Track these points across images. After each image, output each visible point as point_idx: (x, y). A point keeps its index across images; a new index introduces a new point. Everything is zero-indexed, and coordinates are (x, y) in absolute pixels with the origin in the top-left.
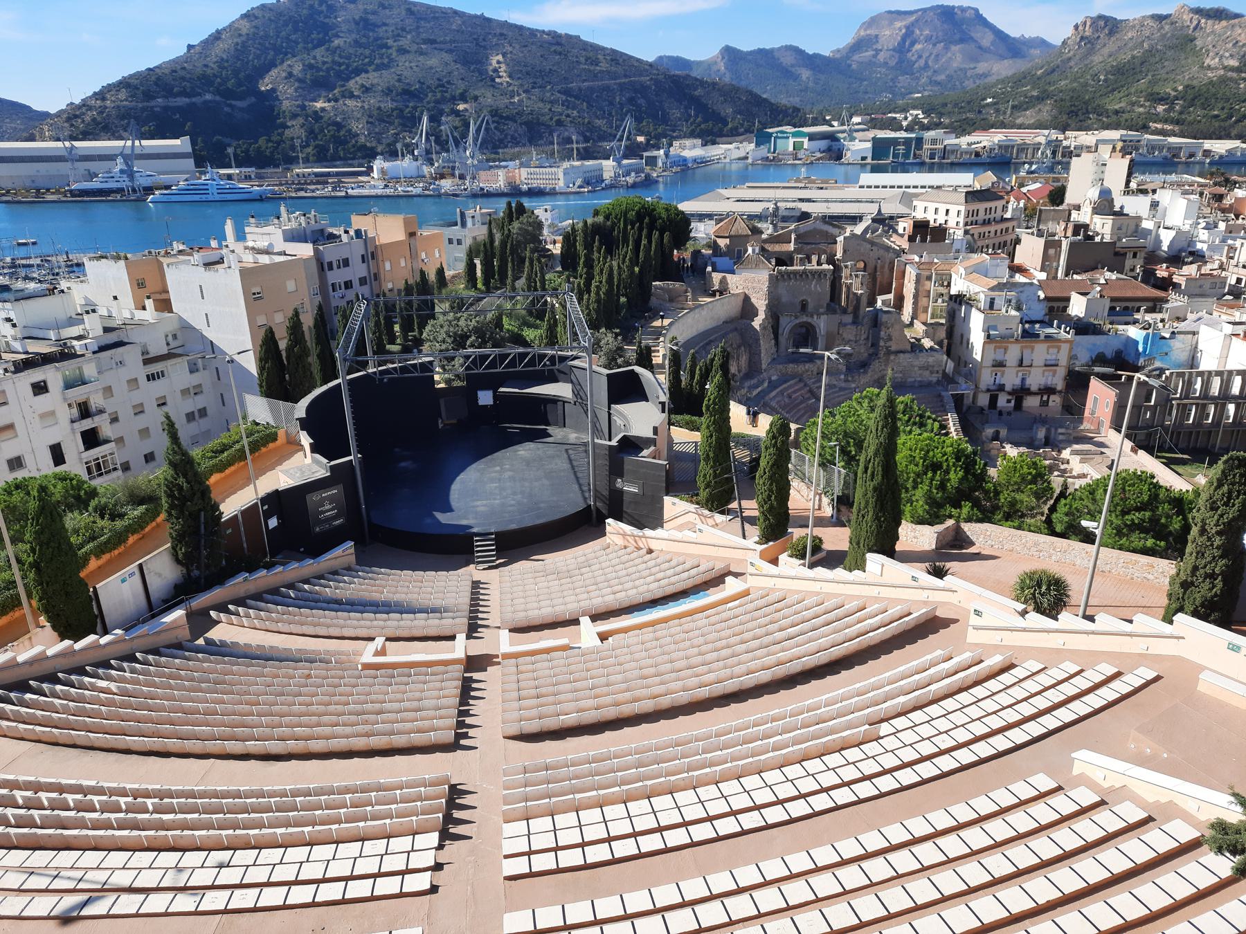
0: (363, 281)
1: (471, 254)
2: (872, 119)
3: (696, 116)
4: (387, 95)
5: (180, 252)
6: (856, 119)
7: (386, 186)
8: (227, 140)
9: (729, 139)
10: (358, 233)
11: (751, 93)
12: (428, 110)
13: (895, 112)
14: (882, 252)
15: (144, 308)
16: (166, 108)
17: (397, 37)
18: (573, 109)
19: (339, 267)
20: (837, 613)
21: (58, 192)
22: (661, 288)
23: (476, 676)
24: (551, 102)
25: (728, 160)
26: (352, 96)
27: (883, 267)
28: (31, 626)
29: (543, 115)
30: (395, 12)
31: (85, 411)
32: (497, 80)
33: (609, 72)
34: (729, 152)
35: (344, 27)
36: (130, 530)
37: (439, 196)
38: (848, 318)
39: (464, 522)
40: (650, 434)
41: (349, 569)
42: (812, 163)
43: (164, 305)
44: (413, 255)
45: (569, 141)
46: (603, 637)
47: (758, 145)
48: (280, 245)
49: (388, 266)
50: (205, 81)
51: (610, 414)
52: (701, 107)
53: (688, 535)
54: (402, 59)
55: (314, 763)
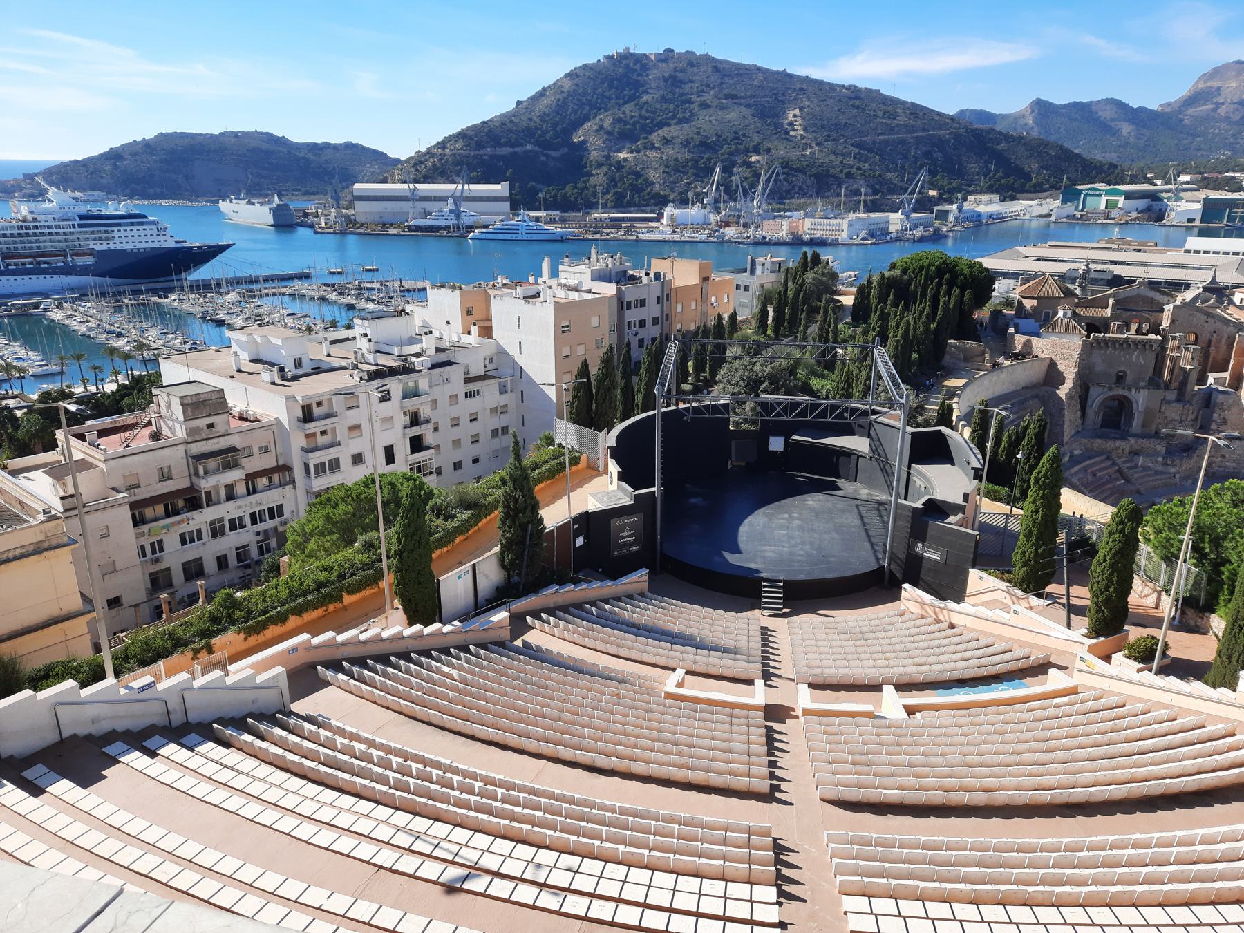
0: (655, 321)
1: (766, 299)
2: (1205, 179)
3: (997, 171)
4: (685, 146)
6: (1184, 178)
7: (674, 232)
8: (539, 186)
9: (1031, 195)
10: (657, 276)
11: (1062, 148)
13: (1234, 171)
14: (1219, 325)
15: (469, 333)
16: (492, 157)
17: (700, 93)
18: (865, 161)
20: (1195, 735)
21: (399, 227)
22: (955, 346)
23: (776, 726)
24: (842, 155)
25: (1027, 217)
26: (653, 147)
27: (1219, 342)
28: (388, 606)
31: (415, 420)
32: (792, 133)
33: (906, 126)
34: (1028, 208)
35: (654, 84)
36: (458, 531)
37: (723, 242)
38: (1172, 395)
39: (753, 566)
40: (960, 501)
41: (642, 595)
42: (1126, 223)
43: (487, 332)
44: (704, 297)
45: (857, 193)
46: (910, 710)
47: (1064, 202)
48: (588, 283)
49: (679, 308)
50: (529, 133)
51: (909, 474)
52: (1002, 160)
53: (999, 614)
54: (703, 112)
55: (635, 784)
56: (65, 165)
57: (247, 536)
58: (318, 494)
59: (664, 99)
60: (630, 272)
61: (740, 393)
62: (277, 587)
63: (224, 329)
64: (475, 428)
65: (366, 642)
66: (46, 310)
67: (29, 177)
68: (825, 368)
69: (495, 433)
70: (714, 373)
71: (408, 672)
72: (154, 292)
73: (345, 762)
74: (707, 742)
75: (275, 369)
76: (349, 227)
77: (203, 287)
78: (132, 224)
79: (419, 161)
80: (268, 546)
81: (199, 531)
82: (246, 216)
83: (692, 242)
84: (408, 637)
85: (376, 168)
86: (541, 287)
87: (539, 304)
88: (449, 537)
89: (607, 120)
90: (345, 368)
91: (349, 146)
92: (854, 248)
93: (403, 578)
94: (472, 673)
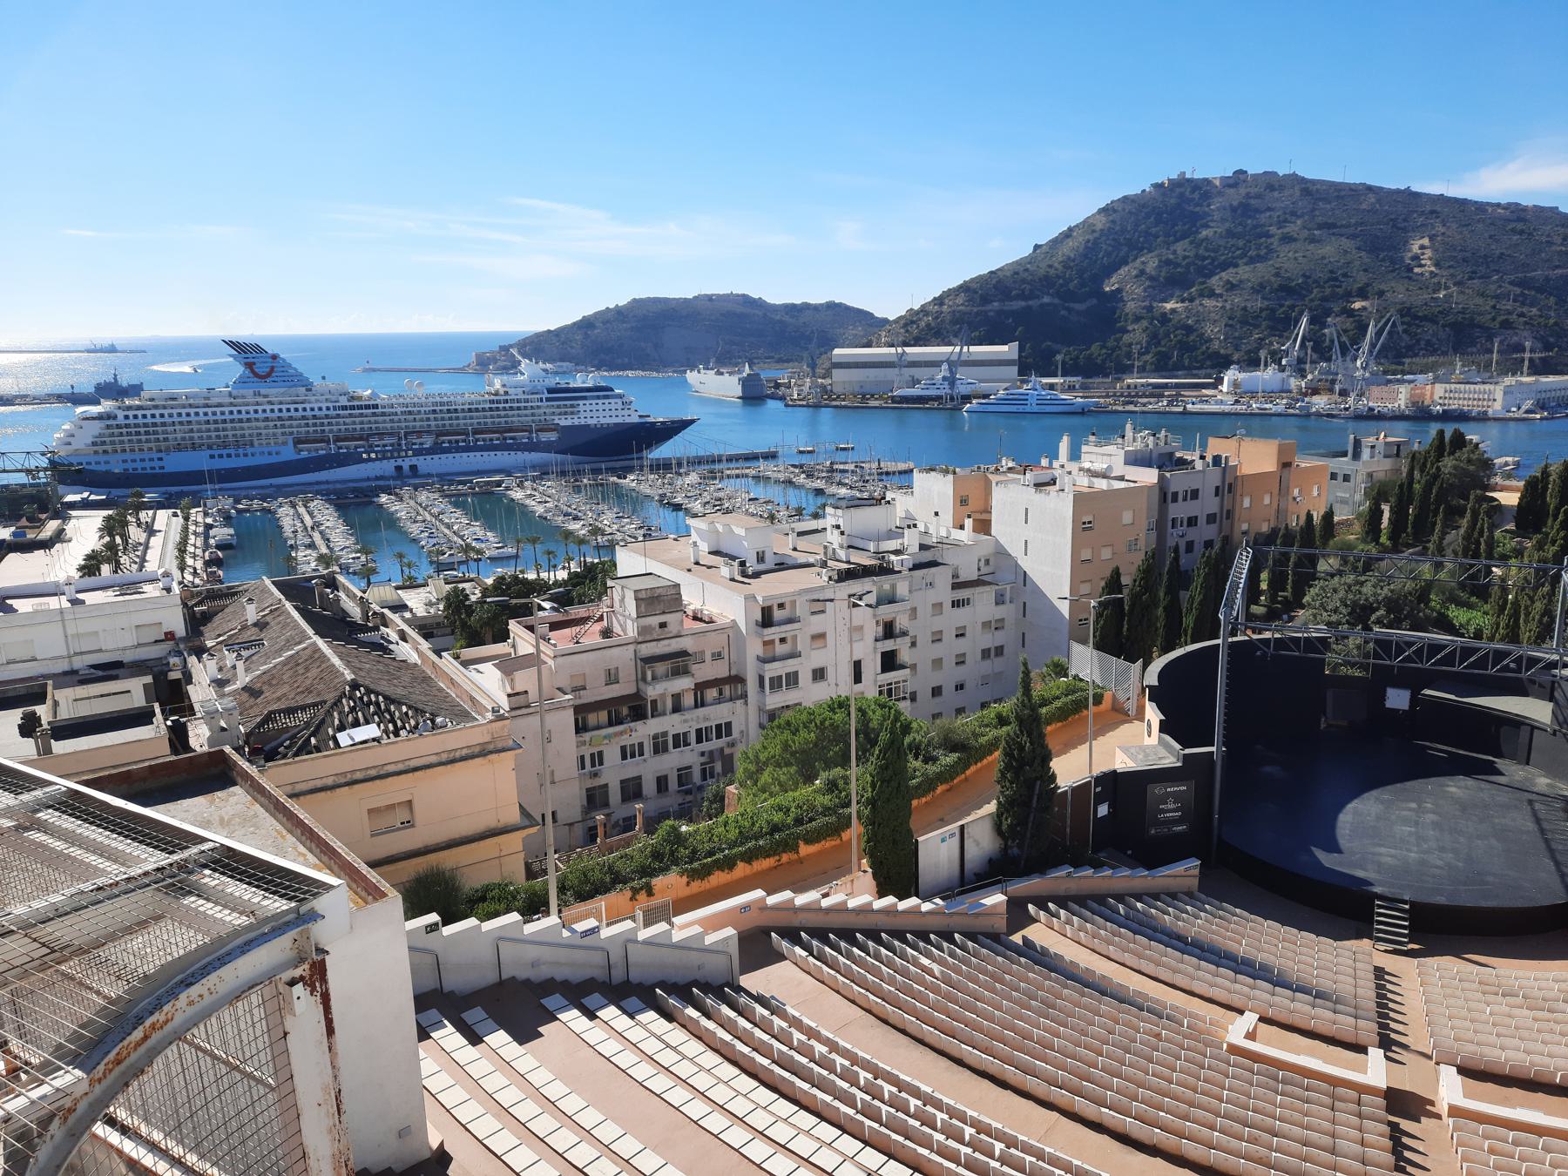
0: (1211, 519)
1: (1378, 493)
5: (1010, 469)
7: (1237, 402)
8: (1059, 346)
12: (1311, 310)
15: (962, 527)
16: (999, 313)
17: (1281, 223)
18: (1532, 305)
19: (1185, 499)
21: (881, 398)
23: (1405, 1125)
24: (1497, 297)
26: (1212, 294)
28: (855, 867)
29: (1480, 314)
30: (1287, 193)
31: (889, 631)
32: (1417, 270)
36: (942, 777)
37: (1308, 415)
39: (1360, 874)
41: (1190, 894)
43: (983, 526)
48: (1119, 468)
49: (1247, 503)
50: (1047, 282)
54: (1286, 248)
56: (538, 335)
57: (689, 757)
58: (772, 716)
59: (1230, 234)
60: (1178, 455)
61: (1339, 623)
62: (726, 824)
63: (681, 514)
64: (962, 646)
65: (829, 910)
66: (508, 489)
67: (505, 349)
68: (1472, 594)
69: (986, 654)
70: (1299, 593)
71: (877, 957)
72: (613, 471)
73: (804, 1067)
74: (1296, 1130)
75: (736, 564)
76: (825, 399)
77: (663, 467)
78: (598, 397)
79: (910, 319)
80: (712, 769)
81: (641, 745)
82: (716, 385)
83: (1264, 415)
84: (879, 911)
85: (860, 330)
86: (1057, 473)
87: (1053, 494)
88: (929, 784)
89: (1151, 263)
90: (812, 565)
91: (831, 306)
92: (1512, 424)
93: (875, 834)
94: (958, 972)
